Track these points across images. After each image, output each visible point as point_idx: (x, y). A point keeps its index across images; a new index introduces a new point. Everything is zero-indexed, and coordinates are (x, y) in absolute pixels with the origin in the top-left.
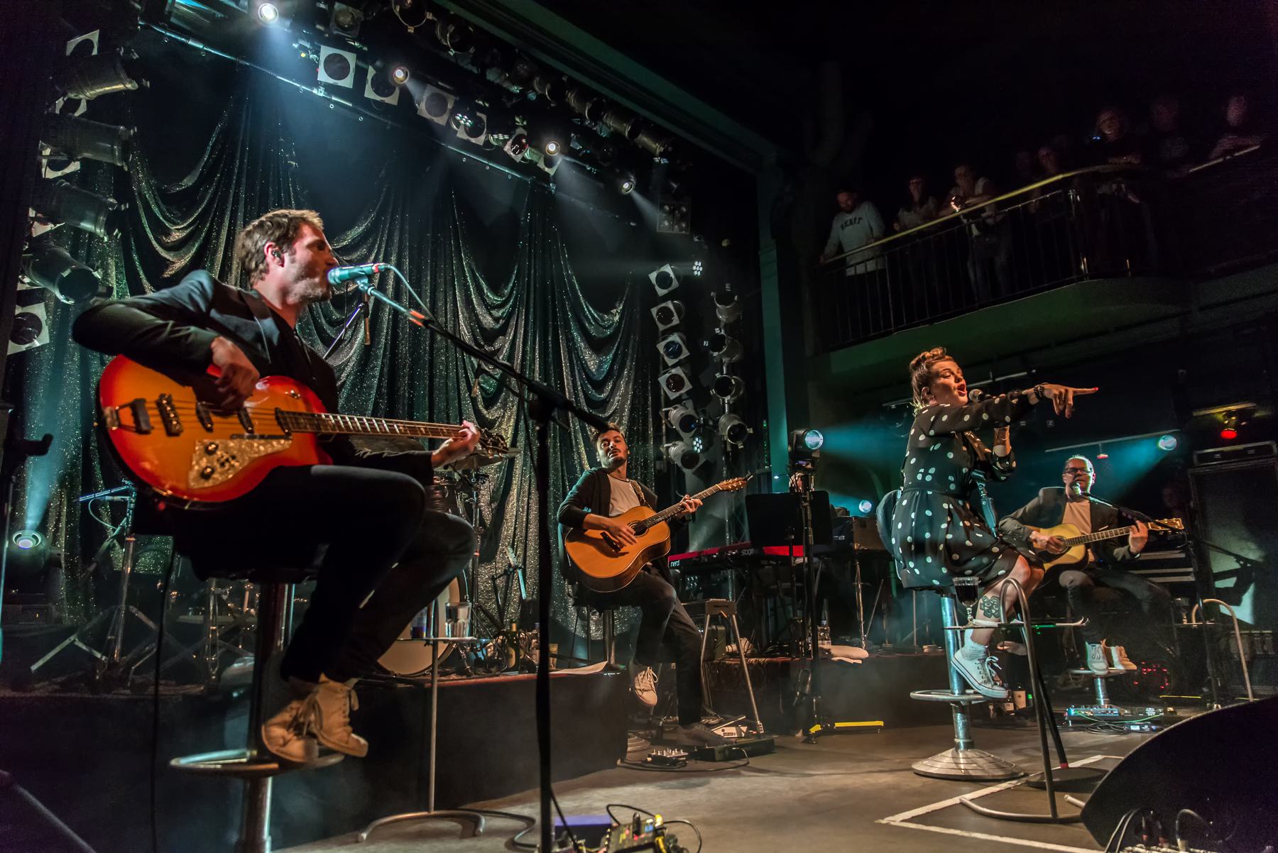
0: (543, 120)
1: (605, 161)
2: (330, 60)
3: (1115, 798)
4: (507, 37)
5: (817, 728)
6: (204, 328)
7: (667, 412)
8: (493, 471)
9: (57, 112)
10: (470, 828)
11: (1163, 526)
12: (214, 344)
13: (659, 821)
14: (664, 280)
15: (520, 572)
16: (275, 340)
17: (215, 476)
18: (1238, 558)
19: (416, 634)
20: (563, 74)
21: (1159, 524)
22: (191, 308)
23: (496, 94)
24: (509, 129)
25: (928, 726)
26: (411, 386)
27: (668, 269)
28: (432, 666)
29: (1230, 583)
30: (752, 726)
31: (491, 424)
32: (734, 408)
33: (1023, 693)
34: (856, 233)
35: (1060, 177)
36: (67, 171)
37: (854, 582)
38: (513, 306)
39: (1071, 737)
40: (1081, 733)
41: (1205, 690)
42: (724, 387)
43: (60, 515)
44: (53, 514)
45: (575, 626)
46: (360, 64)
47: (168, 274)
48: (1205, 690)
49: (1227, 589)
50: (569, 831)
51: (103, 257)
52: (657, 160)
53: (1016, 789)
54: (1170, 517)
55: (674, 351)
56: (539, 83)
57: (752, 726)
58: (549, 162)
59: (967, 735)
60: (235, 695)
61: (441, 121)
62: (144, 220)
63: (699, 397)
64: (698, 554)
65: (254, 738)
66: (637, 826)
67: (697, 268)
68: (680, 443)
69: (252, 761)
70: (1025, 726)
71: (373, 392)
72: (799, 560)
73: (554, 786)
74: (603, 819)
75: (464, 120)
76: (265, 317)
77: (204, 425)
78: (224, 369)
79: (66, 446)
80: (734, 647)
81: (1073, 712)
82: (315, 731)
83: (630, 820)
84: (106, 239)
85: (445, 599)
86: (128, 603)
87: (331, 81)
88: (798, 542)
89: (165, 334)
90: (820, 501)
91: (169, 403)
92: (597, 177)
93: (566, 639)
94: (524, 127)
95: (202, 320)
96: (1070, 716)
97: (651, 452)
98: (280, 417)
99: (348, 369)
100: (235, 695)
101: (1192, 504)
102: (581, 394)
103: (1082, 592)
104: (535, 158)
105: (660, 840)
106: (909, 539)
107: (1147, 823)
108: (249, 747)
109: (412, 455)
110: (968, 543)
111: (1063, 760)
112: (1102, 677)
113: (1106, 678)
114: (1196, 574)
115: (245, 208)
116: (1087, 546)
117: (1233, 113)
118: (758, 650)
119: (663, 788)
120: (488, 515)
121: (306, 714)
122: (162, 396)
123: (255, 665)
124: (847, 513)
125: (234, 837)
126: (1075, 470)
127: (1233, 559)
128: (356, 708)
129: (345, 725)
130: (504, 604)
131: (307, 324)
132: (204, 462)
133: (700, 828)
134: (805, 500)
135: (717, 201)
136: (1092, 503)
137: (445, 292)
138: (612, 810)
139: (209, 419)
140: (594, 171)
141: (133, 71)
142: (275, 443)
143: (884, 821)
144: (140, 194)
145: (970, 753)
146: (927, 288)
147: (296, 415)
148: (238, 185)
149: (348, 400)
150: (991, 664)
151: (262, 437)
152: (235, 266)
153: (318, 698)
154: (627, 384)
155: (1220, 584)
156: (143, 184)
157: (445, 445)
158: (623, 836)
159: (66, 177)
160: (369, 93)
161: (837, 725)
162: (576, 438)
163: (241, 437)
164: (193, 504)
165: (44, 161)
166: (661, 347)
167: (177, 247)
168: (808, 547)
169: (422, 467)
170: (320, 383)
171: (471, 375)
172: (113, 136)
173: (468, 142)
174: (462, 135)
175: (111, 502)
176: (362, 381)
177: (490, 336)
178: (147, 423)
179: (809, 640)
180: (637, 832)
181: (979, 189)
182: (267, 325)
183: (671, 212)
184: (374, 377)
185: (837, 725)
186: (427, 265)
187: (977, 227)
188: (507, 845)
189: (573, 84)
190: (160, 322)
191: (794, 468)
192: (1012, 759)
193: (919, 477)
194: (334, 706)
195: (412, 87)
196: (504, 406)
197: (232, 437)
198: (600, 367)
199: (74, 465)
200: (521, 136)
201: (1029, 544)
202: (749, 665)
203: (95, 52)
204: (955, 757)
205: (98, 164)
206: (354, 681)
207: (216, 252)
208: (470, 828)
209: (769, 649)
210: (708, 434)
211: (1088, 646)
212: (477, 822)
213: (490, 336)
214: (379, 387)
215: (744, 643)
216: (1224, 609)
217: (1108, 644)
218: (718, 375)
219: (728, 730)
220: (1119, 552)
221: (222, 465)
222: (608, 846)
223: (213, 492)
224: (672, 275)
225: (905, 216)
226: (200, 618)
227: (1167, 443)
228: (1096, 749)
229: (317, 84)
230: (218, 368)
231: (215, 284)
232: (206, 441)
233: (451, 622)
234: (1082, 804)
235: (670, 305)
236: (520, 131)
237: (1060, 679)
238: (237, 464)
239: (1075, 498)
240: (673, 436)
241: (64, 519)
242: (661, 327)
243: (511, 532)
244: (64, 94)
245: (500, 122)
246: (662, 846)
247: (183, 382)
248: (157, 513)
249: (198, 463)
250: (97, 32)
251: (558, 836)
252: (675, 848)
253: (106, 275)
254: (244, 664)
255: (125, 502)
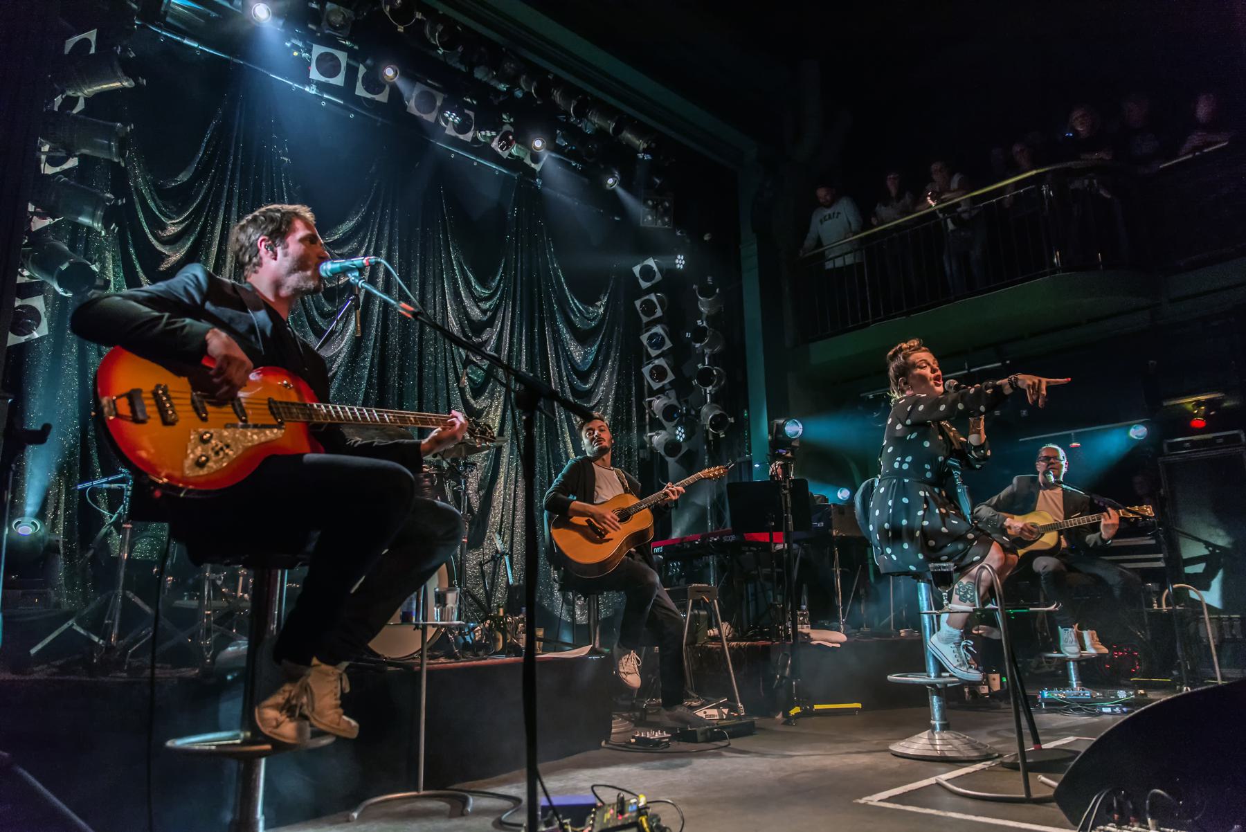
0: (531, 116)
1: (590, 157)
2: (322, 59)
3: (1088, 778)
4: (494, 36)
5: (797, 710)
6: (198, 320)
7: (650, 402)
8: (480, 459)
9: (56, 109)
10: (459, 808)
11: (1134, 513)
12: (208, 336)
13: (642, 801)
14: (647, 273)
15: (507, 558)
16: (268, 332)
17: (210, 464)
18: (1207, 544)
19: (406, 618)
20: (548, 72)
21: (1130, 511)
22: (186, 300)
23: (483, 92)
24: (496, 125)
25: (905, 708)
26: (401, 377)
27: (651, 262)
28: (422, 649)
29: (1199, 568)
30: (733, 708)
31: (478, 414)
32: (715, 398)
33: (997, 676)
34: (835, 228)
35: (1034, 172)
36: (66, 166)
37: (832, 568)
38: (501, 299)
39: (1044, 719)
40: (1054, 715)
41: (1175, 673)
42: (705, 377)
43: (58, 503)
44: (51, 501)
45: (560, 610)
46: (351, 62)
47: (163, 267)
48: (1175, 673)
49: (1196, 574)
50: (555, 810)
51: (100, 250)
52: (640, 156)
53: (990, 769)
54: (1140, 504)
55: (657, 342)
56: (526, 81)
57: (733, 708)
58: (536, 158)
59: (943, 717)
60: (229, 677)
61: (430, 118)
62: (141, 215)
63: (682, 387)
64: (681, 541)
65: (247, 720)
66: (621, 806)
67: (680, 262)
68: (663, 432)
69: (246, 742)
70: (999, 708)
71: (364, 383)
72: (779, 547)
73: (540, 767)
74: (588, 799)
75: (453, 117)
76: (258, 309)
77: (199, 415)
78: (219, 360)
79: (65, 435)
80: (716, 631)
81: (1046, 695)
82: (307, 712)
83: (614, 800)
84: (103, 233)
85: (434, 584)
86: (124, 589)
87: (323, 79)
88: (778, 528)
89: (161, 326)
90: (799, 488)
91: (165, 393)
92: (583, 173)
93: (552, 623)
94: (511, 124)
95: (197, 312)
96: (1043, 698)
97: (635, 441)
98: (273, 407)
99: (339, 360)
100: (229, 677)
101: (1162, 491)
102: (566, 384)
103: (1055, 577)
104: (521, 155)
105: (643, 819)
106: (886, 525)
107: (1118, 802)
108: (243, 728)
109: (402, 444)
110: (944, 529)
111: (1037, 741)
112: (1074, 661)
113: (1078, 661)
114: (1166, 560)
115: (239, 203)
116: (1060, 533)
117: (1203, 110)
118: (739, 634)
119: (646, 768)
120: (475, 502)
121: (298, 696)
122: (158, 386)
123: (249, 649)
124: (826, 500)
125: (228, 817)
126: (1048, 458)
127: (1202, 545)
128: (347, 690)
129: (336, 707)
130: (491, 589)
131: (299, 316)
132: (199, 451)
133: (683, 808)
134: (785, 487)
135: (698, 196)
136: (1064, 491)
137: (434, 285)
138: (597, 790)
139: (204, 408)
140: (579, 167)
141: (129, 69)
142: (268, 432)
143: (862, 801)
144: (136, 189)
145: (946, 735)
146: (903, 281)
147: (289, 405)
148: (232, 181)
149: (339, 390)
150: (966, 647)
151: (255, 426)
152: (229, 259)
153: (310, 680)
154: (611, 374)
155: (1189, 570)
156: (139, 180)
157: (434, 434)
158: (608, 816)
159: (64, 172)
160: (360, 91)
161: (816, 707)
162: (562, 427)
163: (235, 426)
164: (189, 492)
165: (43, 157)
166: (644, 338)
167: (173, 241)
168: (788, 533)
169: (412, 455)
170: (312, 374)
171: (459, 366)
172: (110, 133)
173: (456, 138)
174: (450, 131)
175: (109, 490)
176: (353, 372)
177: (478, 327)
178: (144, 412)
179: (789, 624)
180: (621, 811)
181: (956, 179)
182: (260, 317)
183: (654, 207)
184: (365, 367)
185: (816, 707)
186: (417, 259)
187: (953, 222)
188: (494, 824)
189: (559, 82)
190: (156, 314)
191: (774, 457)
192: (986, 740)
193: (896, 465)
194: (326, 689)
195: (402, 85)
196: (492, 396)
197: (226, 427)
198: (585, 358)
199: (72, 454)
200: (508, 133)
201: (1003, 530)
202: (730, 648)
203: (93, 51)
204: (931, 739)
205: (96, 160)
206: (345, 664)
207: (210, 245)
208: (459, 808)
209: (750, 633)
210: (691, 423)
211: (1061, 630)
212: (465, 802)
213: (478, 327)
214: (370, 377)
215: (725, 628)
216: (1193, 594)
217: (1081, 628)
218: (700, 366)
219: (710, 712)
220: (1091, 538)
221: (217, 453)
222: (592, 825)
223: (208, 480)
224: (655, 268)
225: (882, 211)
226: (194, 603)
227: (1138, 432)
228: (1069, 730)
229: (309, 82)
230: (213, 359)
231: (210, 277)
232: (201, 430)
233: (439, 607)
234: (1055, 784)
235: (653, 297)
236: (507, 128)
237: (1034, 662)
238: (231, 453)
239: (1048, 486)
240: (656, 425)
241: (62, 506)
242: (645, 319)
243: (498, 519)
244: (63, 93)
245: (488, 119)
246: (645, 825)
247: (178, 372)
248: (153, 501)
249: (193, 452)
250: (94, 32)
251: (544, 815)
252: (658, 827)
253: (103, 268)
254: (238, 648)
255: (122, 490)
